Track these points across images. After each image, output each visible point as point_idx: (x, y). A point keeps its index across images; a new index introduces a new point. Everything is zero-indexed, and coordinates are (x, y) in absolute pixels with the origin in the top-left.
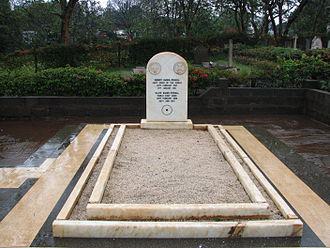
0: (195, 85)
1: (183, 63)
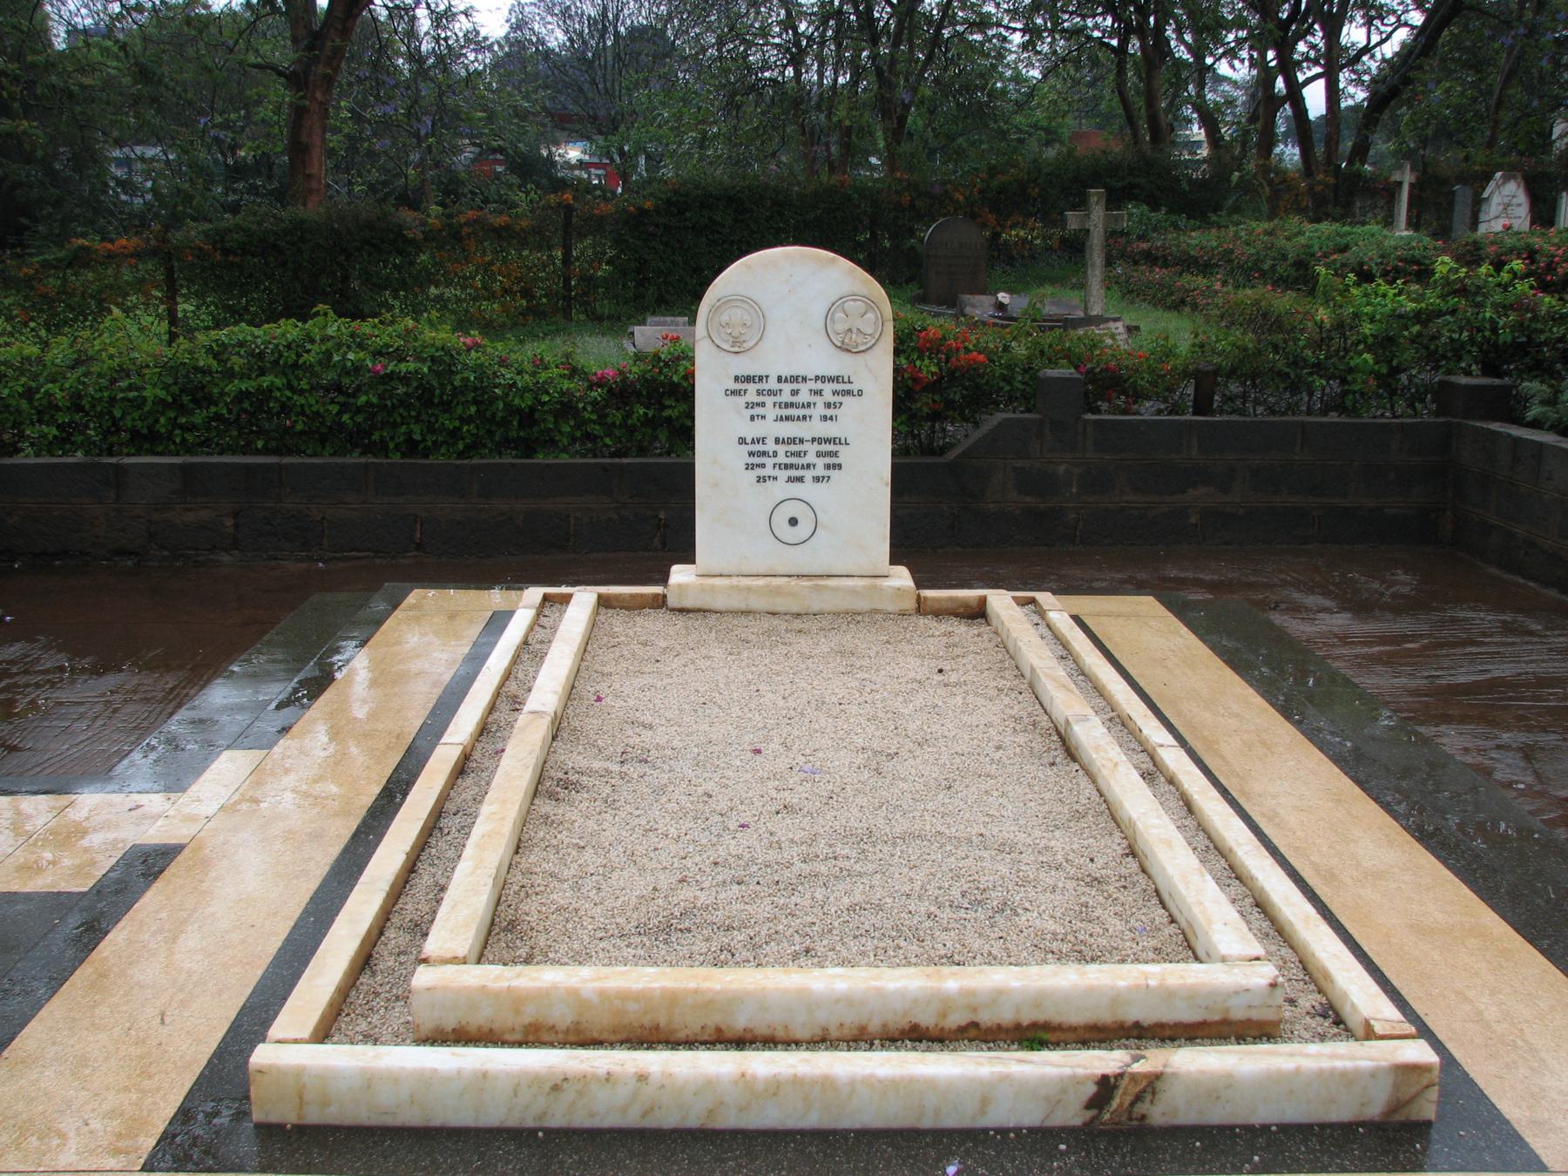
0: (924, 404)
1: (871, 304)
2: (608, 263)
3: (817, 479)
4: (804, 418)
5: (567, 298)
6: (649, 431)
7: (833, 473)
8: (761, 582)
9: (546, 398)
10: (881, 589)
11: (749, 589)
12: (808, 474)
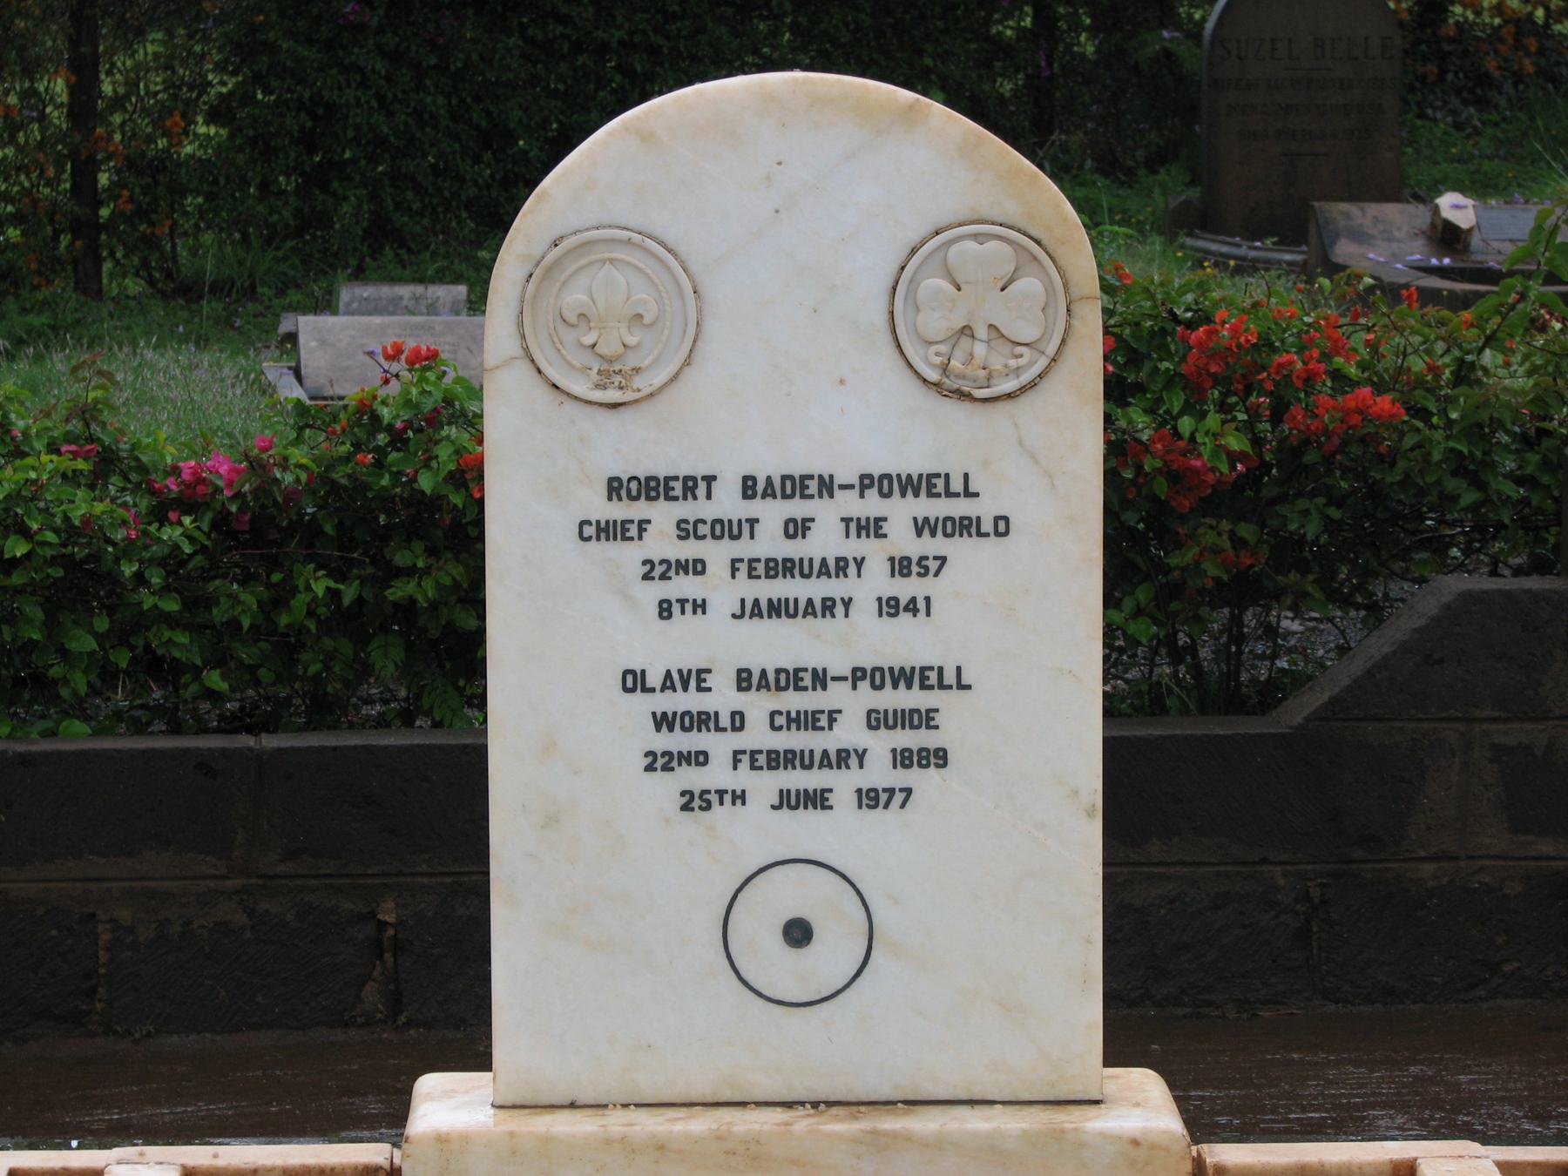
0: (1207, 549)
1: (1034, 248)
2: (213, 117)
3: (870, 799)
4: (828, 606)
5: (86, 228)
6: (346, 648)
7: (923, 780)
8: (700, 1124)
9: (20, 549)
10: (1080, 1144)
11: (661, 1147)
12: (843, 783)
